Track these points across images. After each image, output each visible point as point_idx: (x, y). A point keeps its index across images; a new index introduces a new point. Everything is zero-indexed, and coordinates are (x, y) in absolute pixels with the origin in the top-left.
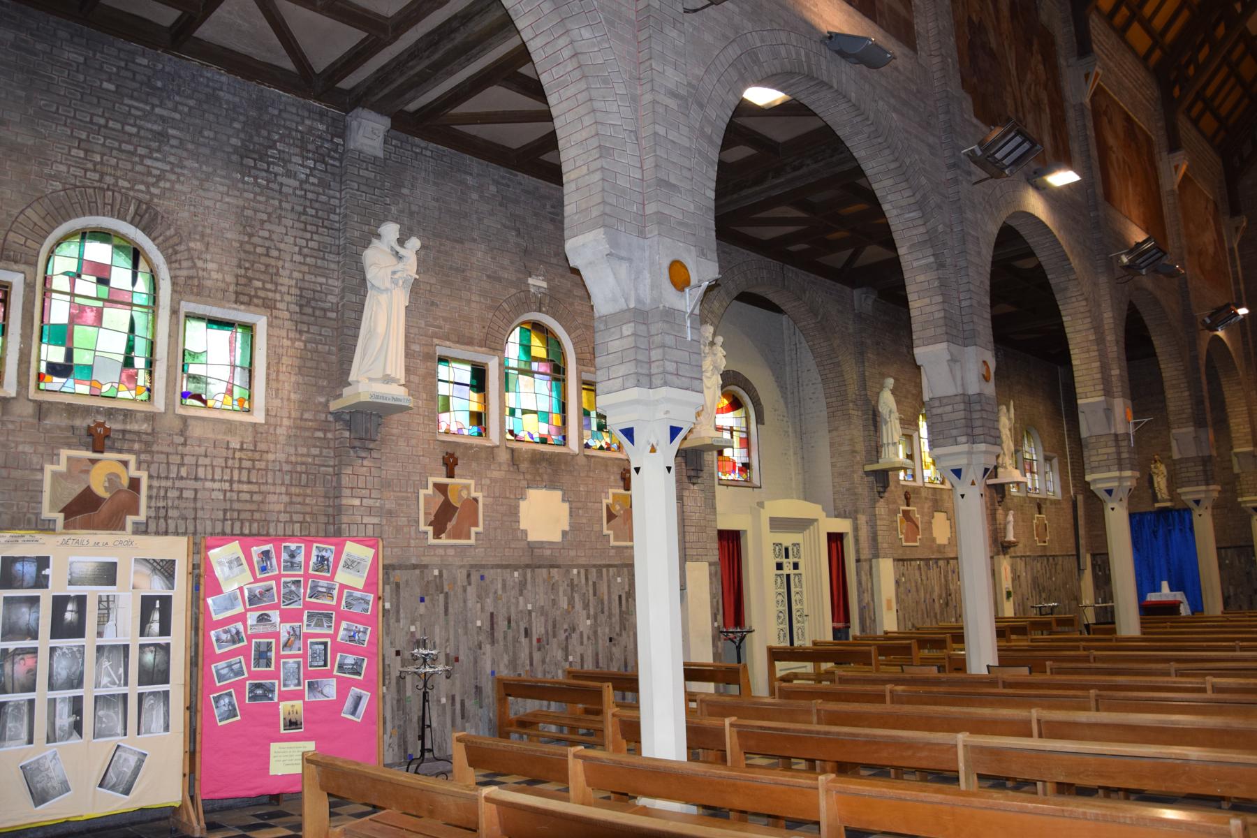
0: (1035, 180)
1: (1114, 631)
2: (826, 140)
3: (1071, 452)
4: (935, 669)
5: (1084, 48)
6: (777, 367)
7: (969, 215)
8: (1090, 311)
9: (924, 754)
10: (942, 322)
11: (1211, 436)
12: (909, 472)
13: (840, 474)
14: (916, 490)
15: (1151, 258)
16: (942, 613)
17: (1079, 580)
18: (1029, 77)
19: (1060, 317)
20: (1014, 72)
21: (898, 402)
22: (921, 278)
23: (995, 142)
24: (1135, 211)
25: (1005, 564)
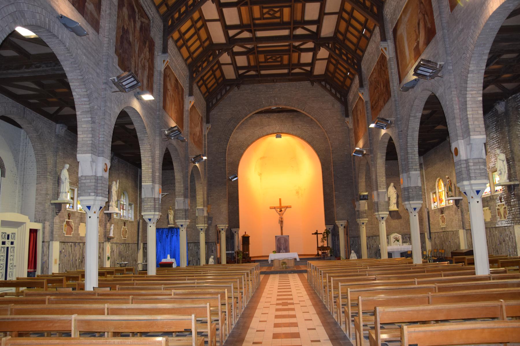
0: (138, 96)
1: (146, 273)
2: (51, 59)
3: (137, 203)
4: (71, 289)
5: (165, 50)
6: (15, 152)
7: (108, 104)
9: (57, 325)
10: (90, 145)
11: (189, 202)
12: (71, 205)
13: (39, 203)
14: (73, 213)
15: (176, 133)
16: (79, 265)
17: (137, 253)
19: (140, 150)
20: (137, 52)
21: (70, 175)
22: (84, 126)
23: (124, 77)
24: (174, 115)
25: (108, 246)
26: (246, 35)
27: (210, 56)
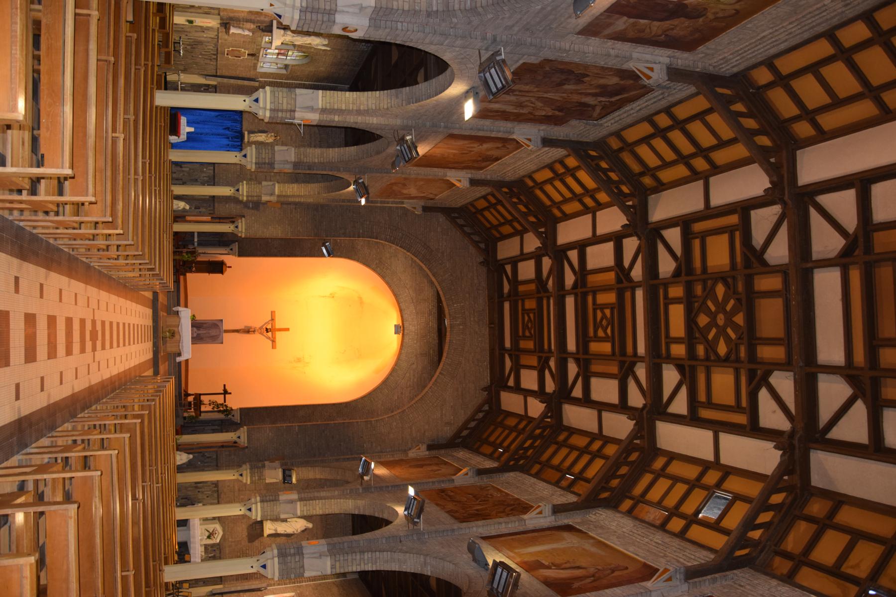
0: (471, 92)
1: (159, 88)
3: (288, 80)
5: (547, 142)
7: (459, 42)
8: (380, 109)
10: (390, 6)
15: (407, 155)
18: (539, 104)
20: (545, 95)
23: (503, 72)
24: (438, 151)
25: (212, 22)
26: (570, 279)
27: (535, 217)
